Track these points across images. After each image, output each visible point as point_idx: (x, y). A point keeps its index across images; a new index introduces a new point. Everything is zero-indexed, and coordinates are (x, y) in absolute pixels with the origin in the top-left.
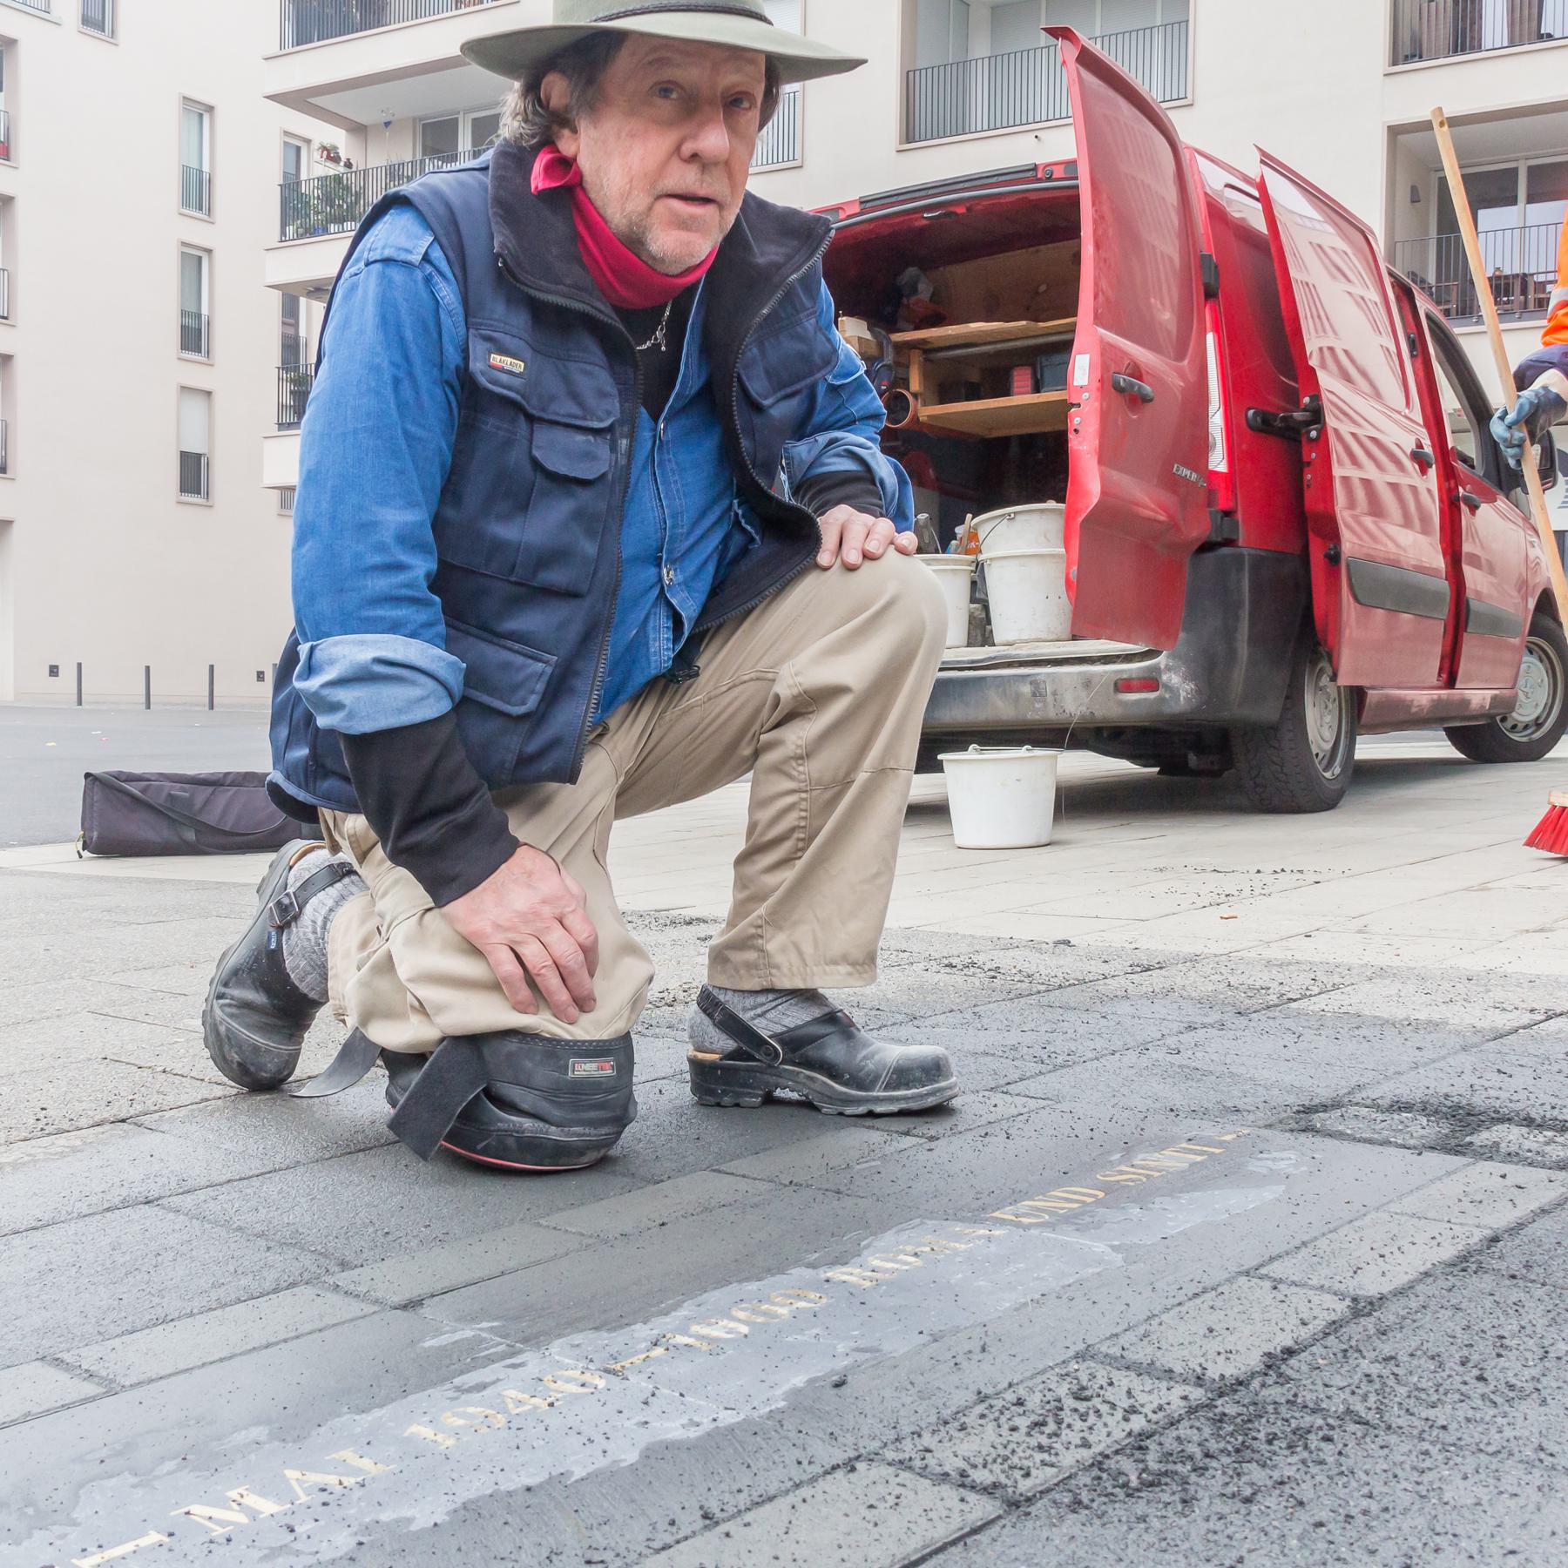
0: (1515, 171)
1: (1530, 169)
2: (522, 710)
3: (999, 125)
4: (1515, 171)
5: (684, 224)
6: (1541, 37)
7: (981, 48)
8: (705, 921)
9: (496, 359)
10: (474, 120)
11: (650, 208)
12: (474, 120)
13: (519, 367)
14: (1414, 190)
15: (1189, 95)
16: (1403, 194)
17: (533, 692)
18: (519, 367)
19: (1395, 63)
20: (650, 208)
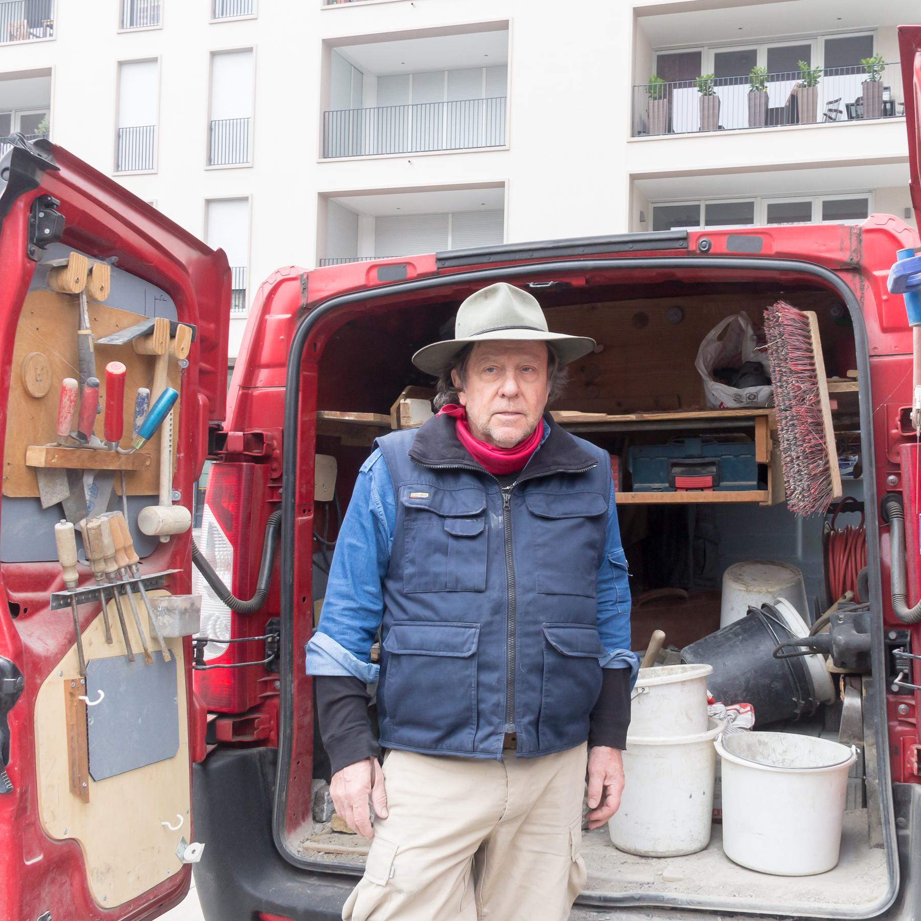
0: (699, 206)
1: (708, 207)
2: (470, 653)
3: (383, 152)
4: (699, 206)
5: (506, 424)
6: (720, 128)
7: (370, 102)
8: (250, 514)
9: (413, 495)
10: (22, 117)
11: (489, 421)
12: (22, 117)
13: (426, 495)
14: (642, 214)
15: (507, 143)
16: (637, 217)
17: (473, 643)
18: (426, 495)
19: (633, 136)
20: (489, 421)
